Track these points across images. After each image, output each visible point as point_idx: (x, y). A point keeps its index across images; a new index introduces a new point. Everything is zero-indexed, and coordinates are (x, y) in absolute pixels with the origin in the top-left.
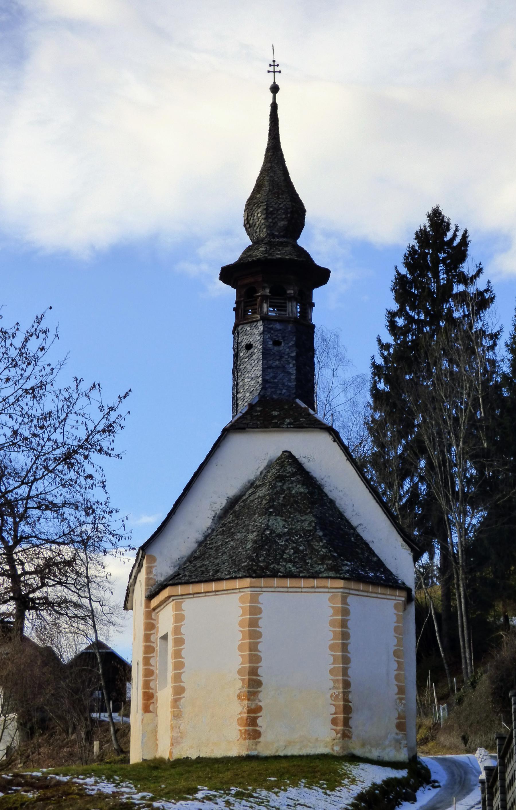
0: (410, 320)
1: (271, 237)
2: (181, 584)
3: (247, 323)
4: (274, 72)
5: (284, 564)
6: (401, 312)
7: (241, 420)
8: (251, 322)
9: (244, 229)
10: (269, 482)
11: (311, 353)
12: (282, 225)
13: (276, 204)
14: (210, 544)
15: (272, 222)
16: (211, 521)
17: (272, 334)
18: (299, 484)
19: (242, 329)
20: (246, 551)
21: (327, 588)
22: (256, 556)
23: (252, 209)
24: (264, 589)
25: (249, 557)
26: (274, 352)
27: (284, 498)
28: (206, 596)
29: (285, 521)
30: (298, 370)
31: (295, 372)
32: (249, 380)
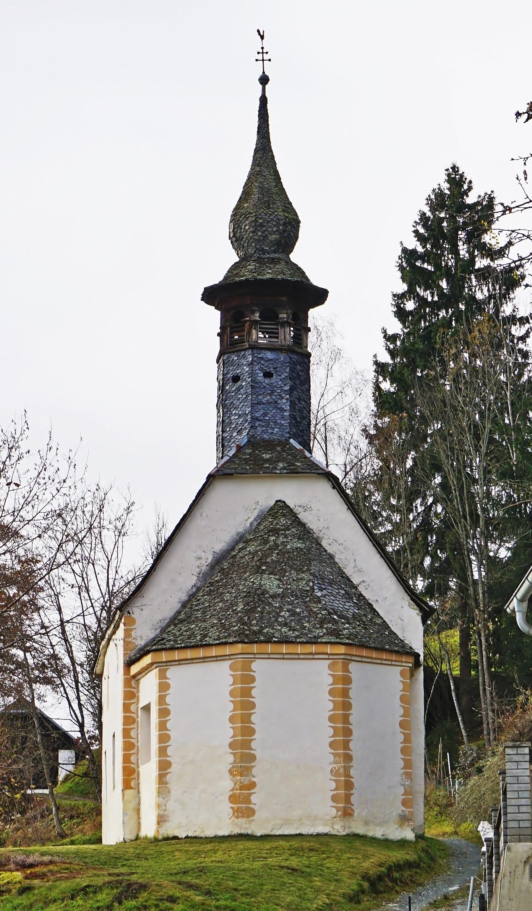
0: (422, 302)
1: (261, 253)
2: (165, 649)
3: (233, 352)
4: (263, 60)
5: (280, 628)
6: (411, 293)
7: (228, 464)
8: (238, 351)
9: (230, 241)
10: (261, 536)
11: (307, 386)
12: (273, 239)
13: (266, 215)
14: (196, 606)
15: (261, 236)
16: (196, 578)
17: (263, 364)
18: (294, 538)
19: (228, 358)
20: (237, 613)
21: (327, 654)
22: (249, 618)
23: (239, 220)
24: (257, 656)
25: (240, 620)
26: (265, 385)
27: (277, 554)
28: (193, 663)
29: (279, 580)
30: (293, 405)
31: (288, 408)
32: (237, 417)
